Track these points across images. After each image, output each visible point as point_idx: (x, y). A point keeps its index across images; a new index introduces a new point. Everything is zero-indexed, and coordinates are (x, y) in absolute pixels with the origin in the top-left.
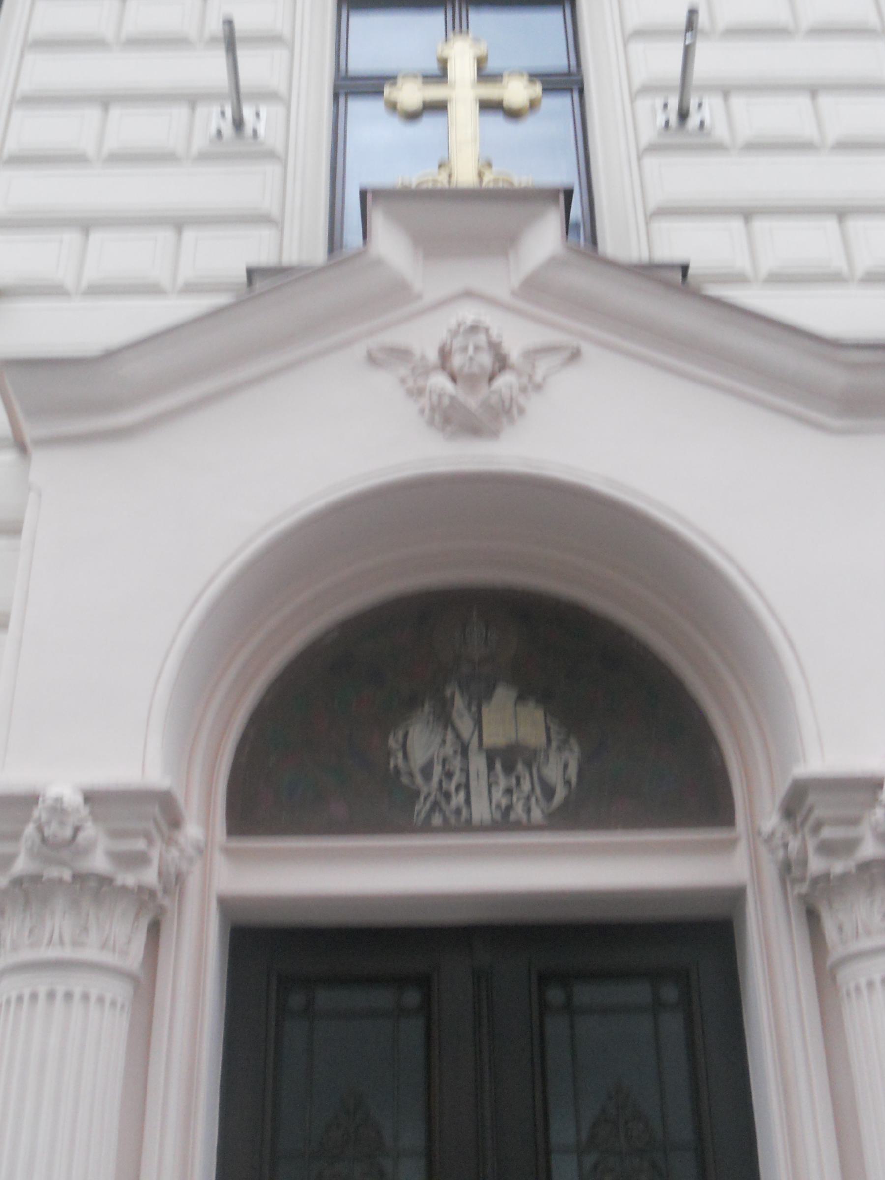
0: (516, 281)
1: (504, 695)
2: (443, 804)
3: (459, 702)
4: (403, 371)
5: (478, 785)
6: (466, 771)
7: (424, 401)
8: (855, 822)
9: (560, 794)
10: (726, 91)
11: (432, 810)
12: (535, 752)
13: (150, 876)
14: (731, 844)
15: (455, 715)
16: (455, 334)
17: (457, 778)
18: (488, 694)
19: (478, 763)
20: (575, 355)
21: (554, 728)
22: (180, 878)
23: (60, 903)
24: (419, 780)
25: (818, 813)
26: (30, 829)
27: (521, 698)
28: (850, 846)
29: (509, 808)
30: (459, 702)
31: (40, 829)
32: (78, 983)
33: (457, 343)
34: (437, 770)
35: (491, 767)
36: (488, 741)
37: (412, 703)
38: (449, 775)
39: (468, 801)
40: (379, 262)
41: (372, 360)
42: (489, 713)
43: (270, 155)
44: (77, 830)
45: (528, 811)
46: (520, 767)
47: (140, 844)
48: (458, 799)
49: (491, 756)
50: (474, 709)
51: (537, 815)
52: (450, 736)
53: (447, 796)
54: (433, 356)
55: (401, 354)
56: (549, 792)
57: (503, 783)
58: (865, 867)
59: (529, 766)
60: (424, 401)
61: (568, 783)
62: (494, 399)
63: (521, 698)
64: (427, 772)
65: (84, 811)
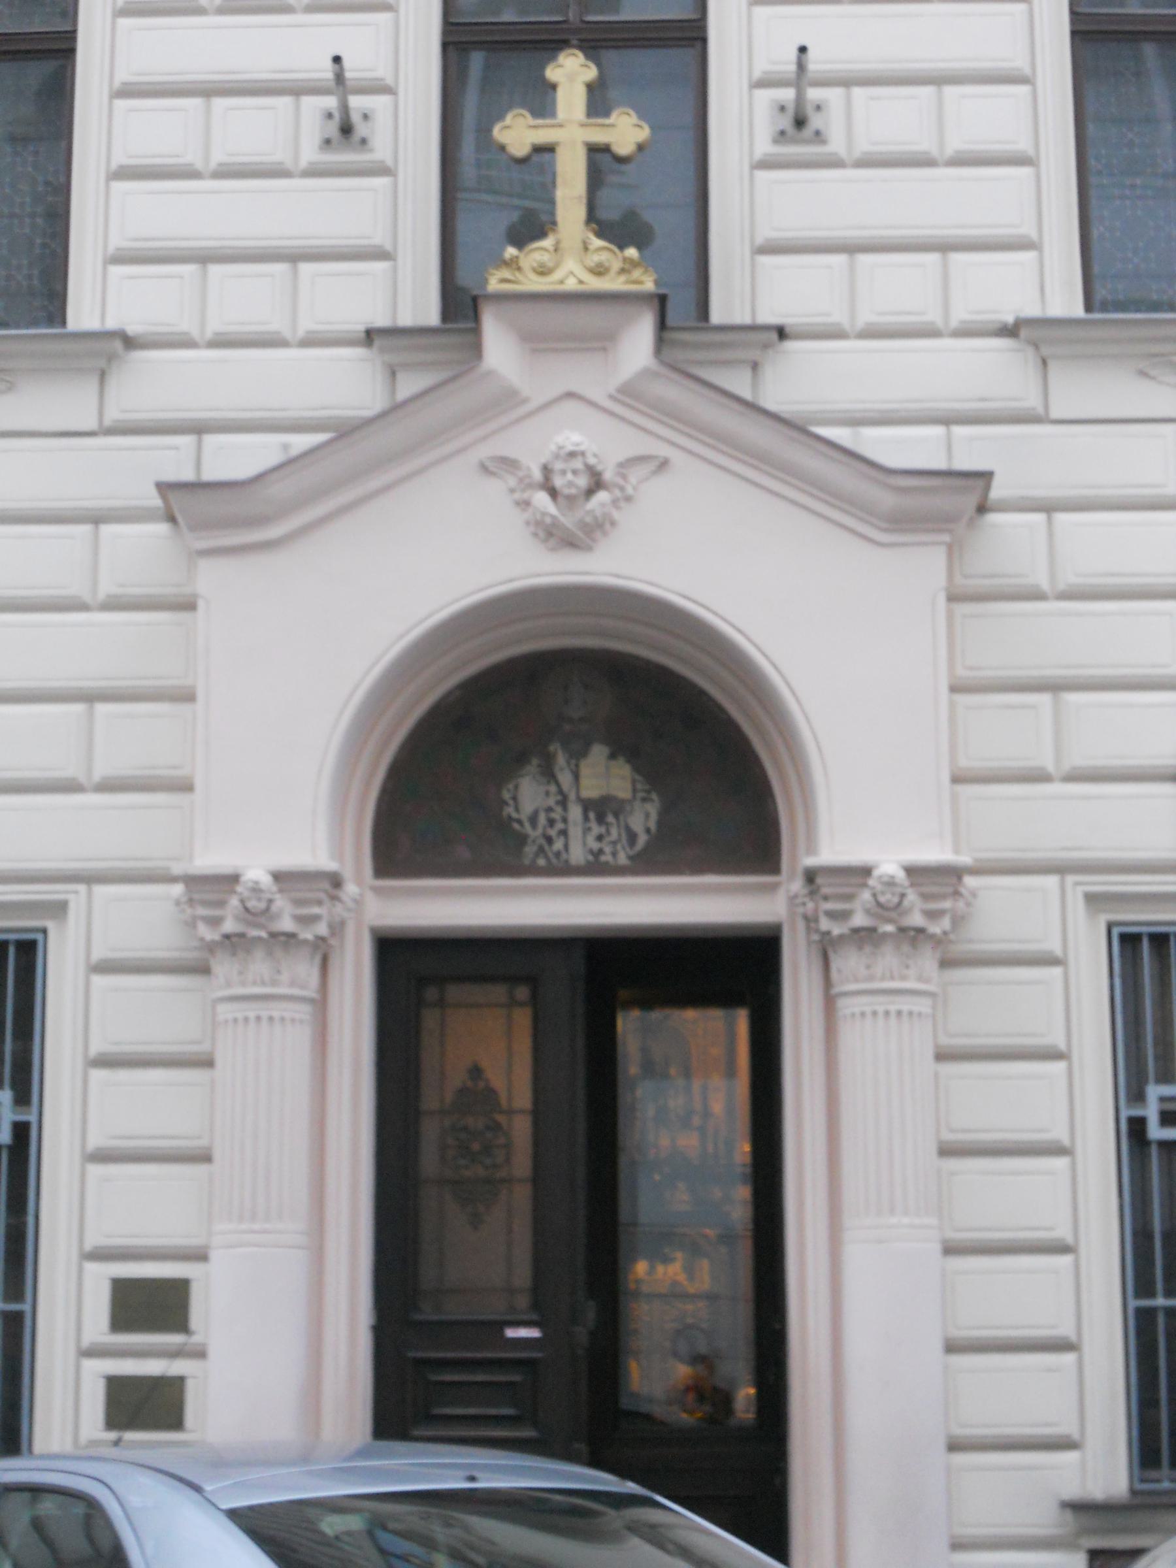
0: (612, 388)
1: (599, 752)
2: (546, 847)
3: (561, 759)
4: (512, 482)
5: (575, 831)
6: (565, 820)
7: (527, 515)
8: (849, 897)
9: (642, 839)
10: (847, 82)
11: (537, 855)
12: (623, 801)
13: (322, 929)
14: (774, 888)
15: (557, 770)
16: (557, 456)
17: (560, 826)
18: (583, 753)
19: (575, 812)
20: (664, 464)
21: (639, 786)
22: (343, 923)
23: (259, 954)
24: (527, 825)
25: (825, 890)
26: (234, 902)
27: (613, 756)
28: (844, 915)
29: (601, 852)
30: (561, 759)
31: (242, 901)
32: (277, 1010)
33: (558, 466)
34: (542, 820)
35: (586, 818)
36: (586, 793)
37: (521, 759)
38: (551, 822)
39: (566, 847)
40: (490, 373)
41: (484, 469)
42: (586, 769)
43: (382, 170)
44: (270, 901)
45: (614, 854)
46: (610, 818)
47: (316, 910)
48: (558, 845)
49: (587, 805)
50: (573, 767)
51: (622, 859)
52: (553, 788)
53: (549, 840)
54: (537, 475)
55: (508, 464)
56: (632, 837)
57: (596, 829)
58: (856, 931)
59: (616, 815)
60: (527, 515)
61: (648, 831)
62: (588, 519)
63: (613, 756)
64: (533, 820)
65: (274, 888)
